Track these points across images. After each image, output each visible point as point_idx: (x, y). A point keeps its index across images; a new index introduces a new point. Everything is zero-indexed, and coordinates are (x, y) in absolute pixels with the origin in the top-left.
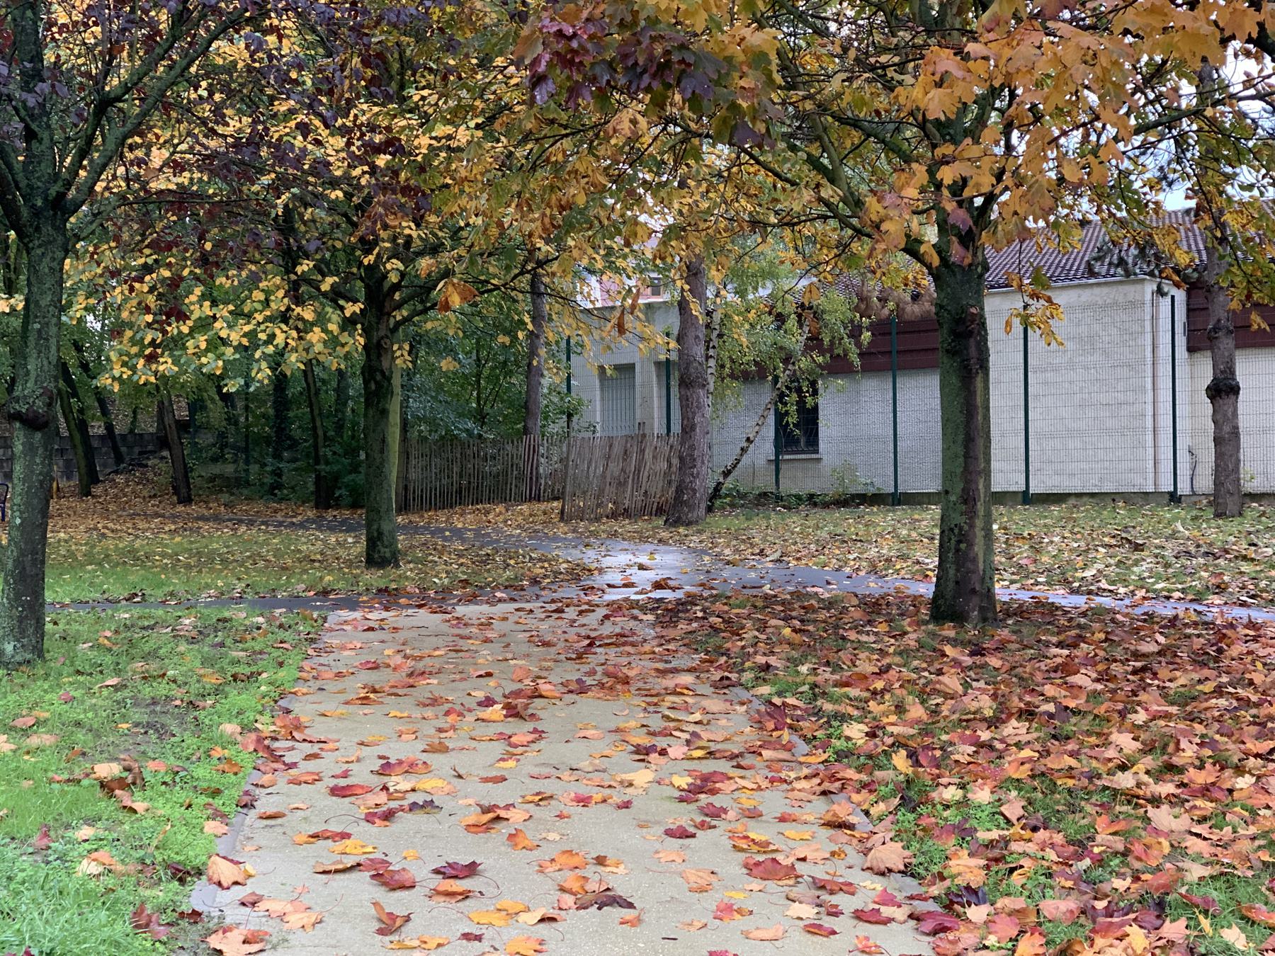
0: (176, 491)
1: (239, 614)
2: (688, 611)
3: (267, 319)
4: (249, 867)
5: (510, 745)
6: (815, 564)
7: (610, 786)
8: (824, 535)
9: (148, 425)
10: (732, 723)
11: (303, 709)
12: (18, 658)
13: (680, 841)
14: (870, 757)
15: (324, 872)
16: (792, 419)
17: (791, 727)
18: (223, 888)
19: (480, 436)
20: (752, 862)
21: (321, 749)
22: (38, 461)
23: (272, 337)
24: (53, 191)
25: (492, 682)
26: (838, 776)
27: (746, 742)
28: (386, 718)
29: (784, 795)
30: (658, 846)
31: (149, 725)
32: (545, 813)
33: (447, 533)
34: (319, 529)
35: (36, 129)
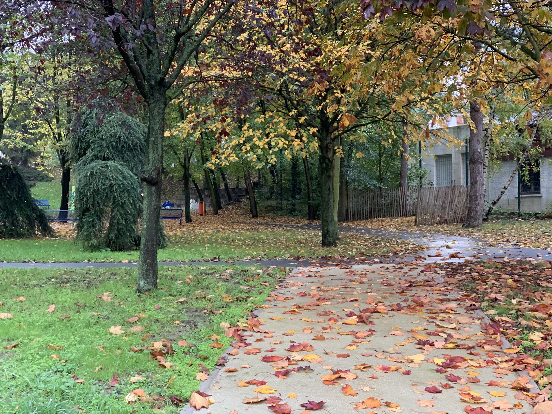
0: (252, 213)
1: (253, 269)
2: (463, 269)
3: (275, 136)
4: (211, 399)
5: (356, 338)
6: (534, 246)
7: (401, 362)
8: (540, 232)
9: (243, 185)
10: (471, 329)
11: (263, 316)
12: (146, 288)
13: (433, 395)
14: (542, 351)
15: (247, 403)
16: (527, 178)
17: (502, 333)
18: (197, 410)
19: (380, 188)
20: (469, 409)
21: (265, 337)
22: (154, 199)
23: (277, 144)
24: (159, 76)
25: (356, 304)
26: (524, 361)
27: (477, 340)
28: (300, 321)
29: (493, 370)
30: (420, 397)
31: (188, 322)
32: (365, 375)
33: (363, 231)
34: (308, 229)
35: (152, 49)
